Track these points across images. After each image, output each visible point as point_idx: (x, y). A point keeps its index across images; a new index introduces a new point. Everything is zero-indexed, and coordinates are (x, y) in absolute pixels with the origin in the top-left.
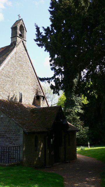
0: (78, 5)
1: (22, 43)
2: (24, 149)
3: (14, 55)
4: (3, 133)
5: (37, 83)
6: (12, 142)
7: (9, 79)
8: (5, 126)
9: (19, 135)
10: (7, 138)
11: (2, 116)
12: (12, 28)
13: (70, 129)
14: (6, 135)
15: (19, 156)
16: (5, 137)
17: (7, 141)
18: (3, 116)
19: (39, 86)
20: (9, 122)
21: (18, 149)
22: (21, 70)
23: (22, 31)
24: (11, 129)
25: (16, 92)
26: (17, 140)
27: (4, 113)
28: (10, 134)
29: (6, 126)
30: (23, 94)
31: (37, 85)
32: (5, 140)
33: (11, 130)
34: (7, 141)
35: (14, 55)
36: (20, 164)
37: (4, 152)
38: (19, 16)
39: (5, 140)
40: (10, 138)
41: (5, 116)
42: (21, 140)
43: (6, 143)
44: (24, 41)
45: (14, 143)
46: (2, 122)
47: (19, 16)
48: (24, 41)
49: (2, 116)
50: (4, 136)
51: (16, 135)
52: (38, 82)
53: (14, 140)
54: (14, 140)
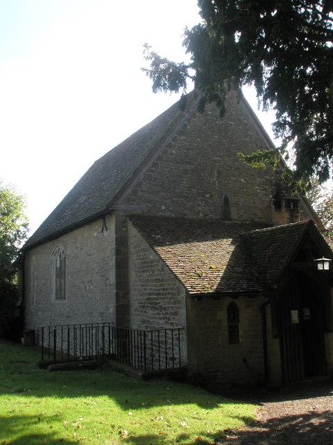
14: (159, 303)
25: (211, 196)
30: (232, 200)
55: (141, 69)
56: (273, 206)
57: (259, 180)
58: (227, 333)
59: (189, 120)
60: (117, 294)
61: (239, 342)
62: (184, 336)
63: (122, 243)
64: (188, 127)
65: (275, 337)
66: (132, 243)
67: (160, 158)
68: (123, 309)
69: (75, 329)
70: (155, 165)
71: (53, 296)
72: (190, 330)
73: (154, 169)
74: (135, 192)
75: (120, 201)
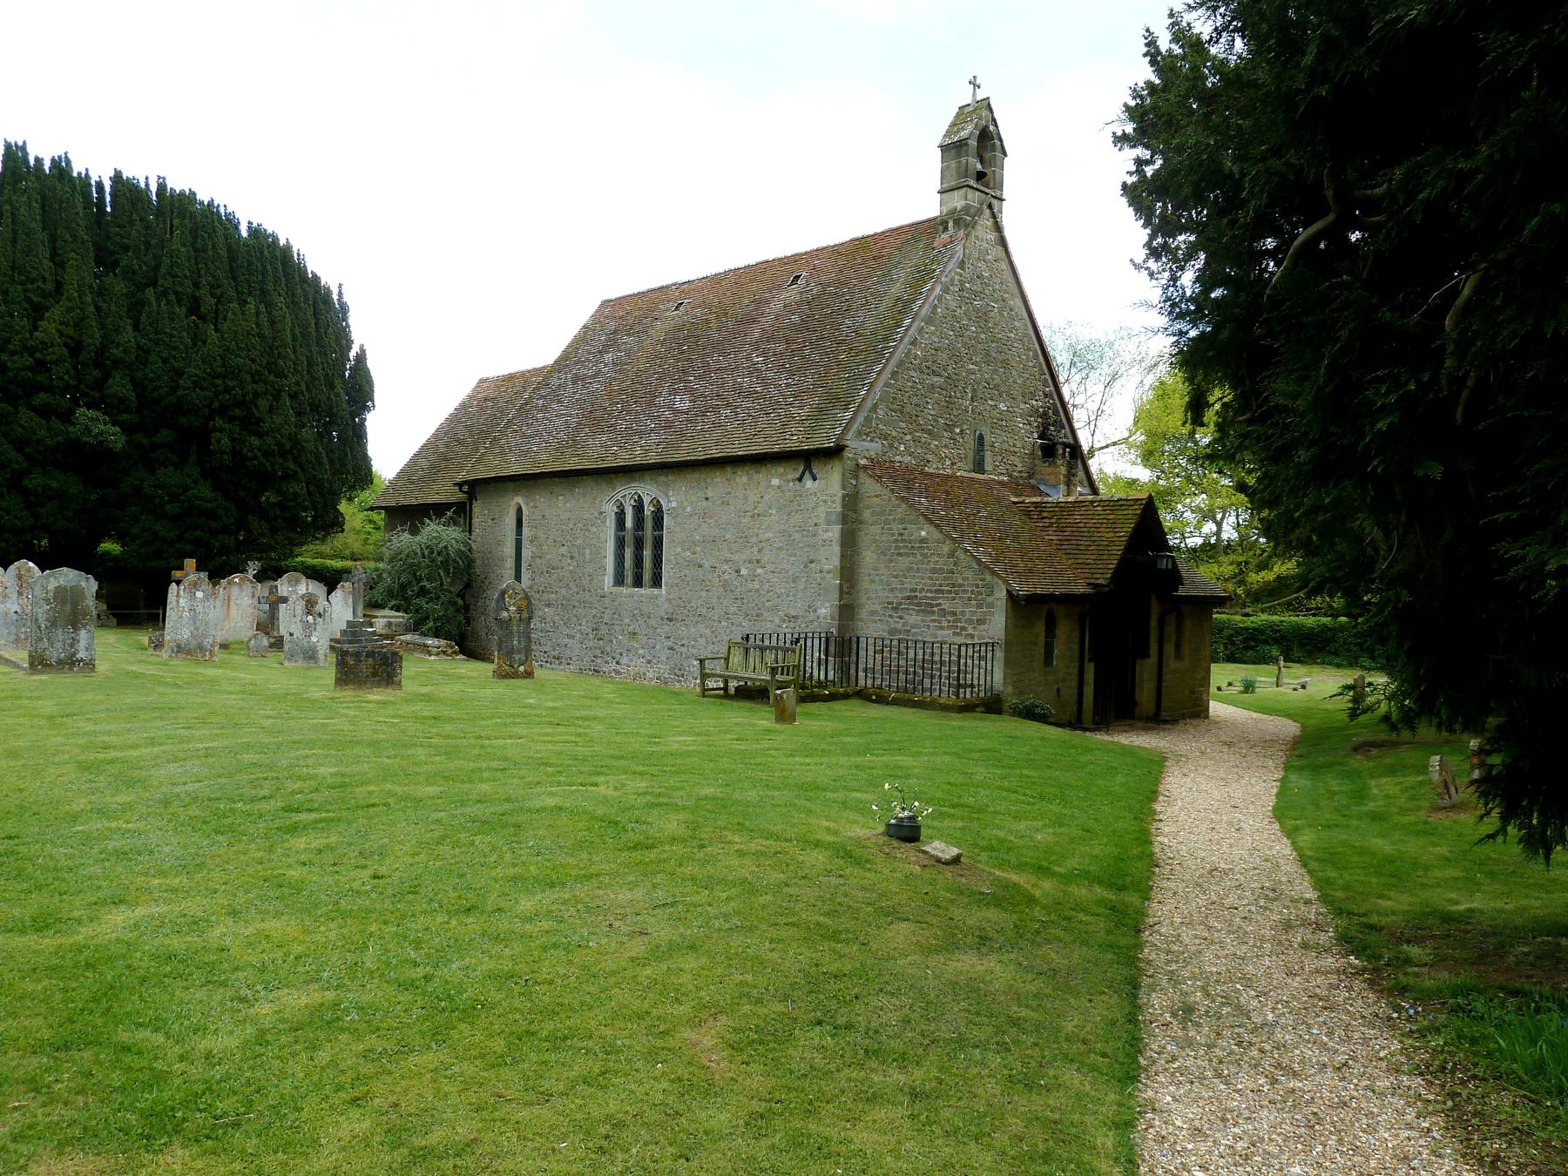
0: (1302, 645)
1: (987, 212)
2: (1535, 822)
3: (956, 273)
4: (928, 595)
5: (1045, 384)
6: (963, 629)
7: (936, 379)
8: (934, 571)
9: (990, 605)
10: (944, 613)
11: (923, 533)
12: (952, 149)
13: (1181, 592)
14: (940, 604)
15: (989, 678)
16: (936, 609)
17: (945, 624)
18: (928, 533)
19: (1056, 397)
20: (951, 555)
21: (989, 655)
22: (983, 336)
23: (987, 156)
24: (960, 581)
25: (962, 432)
26: (980, 622)
27: (931, 522)
28: (954, 599)
29: (941, 571)
30: (988, 438)
31: (1046, 395)
32: (934, 621)
33: (960, 586)
34: (945, 624)
35: (956, 273)
36: (992, 705)
37: (932, 662)
38: (974, 84)
39: (934, 621)
40: (954, 614)
41: (936, 535)
42: (997, 625)
43: (940, 632)
44: (995, 202)
45: (970, 631)
46: (925, 556)
47: (974, 84)
48: (995, 202)
49: (923, 533)
50: (932, 606)
51: (980, 606)
52: (1050, 381)
53: (970, 622)
54: (970, 622)
55: (1131, 260)
56: (1040, 453)
57: (1022, 406)
58: (1042, 651)
59: (940, 298)
60: (841, 585)
61: (1052, 665)
62: (1000, 654)
63: (852, 502)
64: (939, 310)
65: (1090, 661)
66: (868, 507)
67: (901, 363)
68: (847, 611)
69: (827, 639)
70: (894, 373)
71: (609, 579)
72: (1008, 645)
73: (893, 382)
74: (868, 420)
75: (850, 435)
